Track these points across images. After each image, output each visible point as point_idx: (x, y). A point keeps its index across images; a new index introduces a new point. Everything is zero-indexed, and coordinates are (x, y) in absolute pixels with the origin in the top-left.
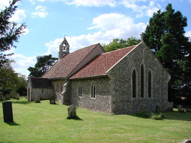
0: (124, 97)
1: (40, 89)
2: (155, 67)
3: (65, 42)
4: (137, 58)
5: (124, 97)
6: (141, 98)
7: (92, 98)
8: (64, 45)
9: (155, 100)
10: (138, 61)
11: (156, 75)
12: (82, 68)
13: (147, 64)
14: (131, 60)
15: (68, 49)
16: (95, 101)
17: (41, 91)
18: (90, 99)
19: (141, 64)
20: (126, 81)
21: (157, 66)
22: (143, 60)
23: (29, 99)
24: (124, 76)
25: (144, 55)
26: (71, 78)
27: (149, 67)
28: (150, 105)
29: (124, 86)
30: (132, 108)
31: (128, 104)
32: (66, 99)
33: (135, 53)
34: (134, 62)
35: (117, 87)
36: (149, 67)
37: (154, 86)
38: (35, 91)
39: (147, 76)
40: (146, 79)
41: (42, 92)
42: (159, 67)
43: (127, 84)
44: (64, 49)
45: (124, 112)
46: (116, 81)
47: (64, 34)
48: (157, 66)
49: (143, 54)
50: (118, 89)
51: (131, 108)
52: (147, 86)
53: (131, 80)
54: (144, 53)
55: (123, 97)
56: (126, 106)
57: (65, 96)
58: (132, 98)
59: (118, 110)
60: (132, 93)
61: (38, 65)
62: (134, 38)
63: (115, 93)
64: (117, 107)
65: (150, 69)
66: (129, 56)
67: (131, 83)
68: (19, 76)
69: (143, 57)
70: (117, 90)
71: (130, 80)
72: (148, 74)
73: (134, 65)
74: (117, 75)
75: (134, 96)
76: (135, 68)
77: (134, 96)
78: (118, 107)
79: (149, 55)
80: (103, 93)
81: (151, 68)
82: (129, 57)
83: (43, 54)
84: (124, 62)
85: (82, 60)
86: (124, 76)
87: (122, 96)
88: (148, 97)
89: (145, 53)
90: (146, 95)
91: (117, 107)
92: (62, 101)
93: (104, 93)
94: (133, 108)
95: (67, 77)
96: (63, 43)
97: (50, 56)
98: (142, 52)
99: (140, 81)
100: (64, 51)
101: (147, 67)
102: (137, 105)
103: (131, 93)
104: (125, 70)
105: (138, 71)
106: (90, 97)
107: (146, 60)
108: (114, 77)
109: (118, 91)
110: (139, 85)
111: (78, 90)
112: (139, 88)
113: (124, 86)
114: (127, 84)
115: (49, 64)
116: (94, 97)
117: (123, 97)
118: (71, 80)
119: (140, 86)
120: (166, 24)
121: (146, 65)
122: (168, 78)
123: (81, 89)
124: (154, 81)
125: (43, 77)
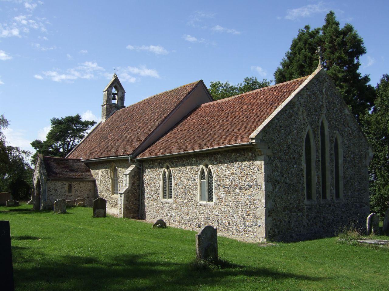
0: (291, 198)
1: (65, 183)
2: (346, 130)
3: (116, 84)
4: (313, 105)
5: (291, 198)
6: (322, 202)
7: (204, 203)
8: (114, 91)
9: (347, 204)
10: (314, 113)
11: (348, 148)
12: (165, 134)
13: (330, 121)
14: (301, 109)
15: (122, 99)
16: (212, 209)
17: (66, 189)
18: (196, 204)
19: (320, 121)
20: (294, 158)
21: (349, 127)
22: (324, 111)
23: (39, 206)
24: (288, 146)
25: (324, 99)
26: (139, 158)
27: (335, 127)
28: (340, 217)
29: (290, 171)
30: (306, 224)
31: (299, 214)
32: (130, 206)
33: (308, 93)
34: (308, 115)
35: (276, 173)
36: (335, 127)
37: (344, 173)
38: (52, 187)
39: (331, 150)
40: (331, 155)
41: (70, 190)
42: (353, 128)
43: (295, 166)
44: (114, 99)
45: (291, 237)
46: (274, 158)
47: (114, 68)
48: (349, 127)
49: (322, 98)
50: (278, 179)
51: (304, 226)
52: (332, 171)
53: (304, 157)
54: (325, 96)
55: (289, 198)
56: (295, 219)
57: (128, 198)
58: (306, 202)
59: (279, 232)
60: (306, 188)
61: (52, 136)
62: (254, 79)
63: (271, 187)
64: (276, 225)
65: (337, 132)
66: (298, 100)
67: (304, 165)
68: (88, 111)
69: (322, 105)
70: (276, 180)
71: (301, 156)
72: (333, 145)
73: (307, 121)
74: (276, 143)
75: (309, 197)
76: (309, 128)
77: (309, 197)
78: (278, 223)
79: (333, 100)
80: (237, 190)
81: (339, 130)
82: (297, 103)
83: (62, 115)
84: (287, 112)
85: (167, 117)
86: (288, 146)
87: (285, 196)
88: (334, 198)
89: (327, 95)
90: (331, 193)
91: (276, 225)
92: (120, 209)
93: (241, 189)
94: (307, 224)
95: (132, 154)
96: (111, 87)
97: (78, 117)
98: (322, 91)
99: (319, 161)
100: (115, 102)
101: (330, 127)
102: (315, 218)
103: (303, 189)
104: (290, 132)
105: (315, 137)
106: (198, 201)
107: (330, 111)
108: (269, 148)
109: (278, 183)
110: (319, 169)
111: (161, 183)
112: (318, 177)
113: (290, 171)
114: (295, 166)
115: (76, 134)
116: (210, 199)
117: (289, 198)
118: (142, 161)
119: (320, 172)
120: (329, 50)
121: (330, 123)
122: (368, 154)
123: (170, 183)
124: (345, 161)
125: (69, 157)
